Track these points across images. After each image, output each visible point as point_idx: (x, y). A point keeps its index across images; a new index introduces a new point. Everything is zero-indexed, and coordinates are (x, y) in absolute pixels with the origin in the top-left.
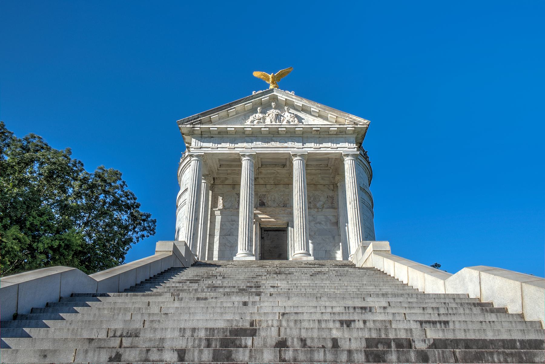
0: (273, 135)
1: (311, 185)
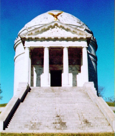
0: (56, 39)
1: (70, 55)
